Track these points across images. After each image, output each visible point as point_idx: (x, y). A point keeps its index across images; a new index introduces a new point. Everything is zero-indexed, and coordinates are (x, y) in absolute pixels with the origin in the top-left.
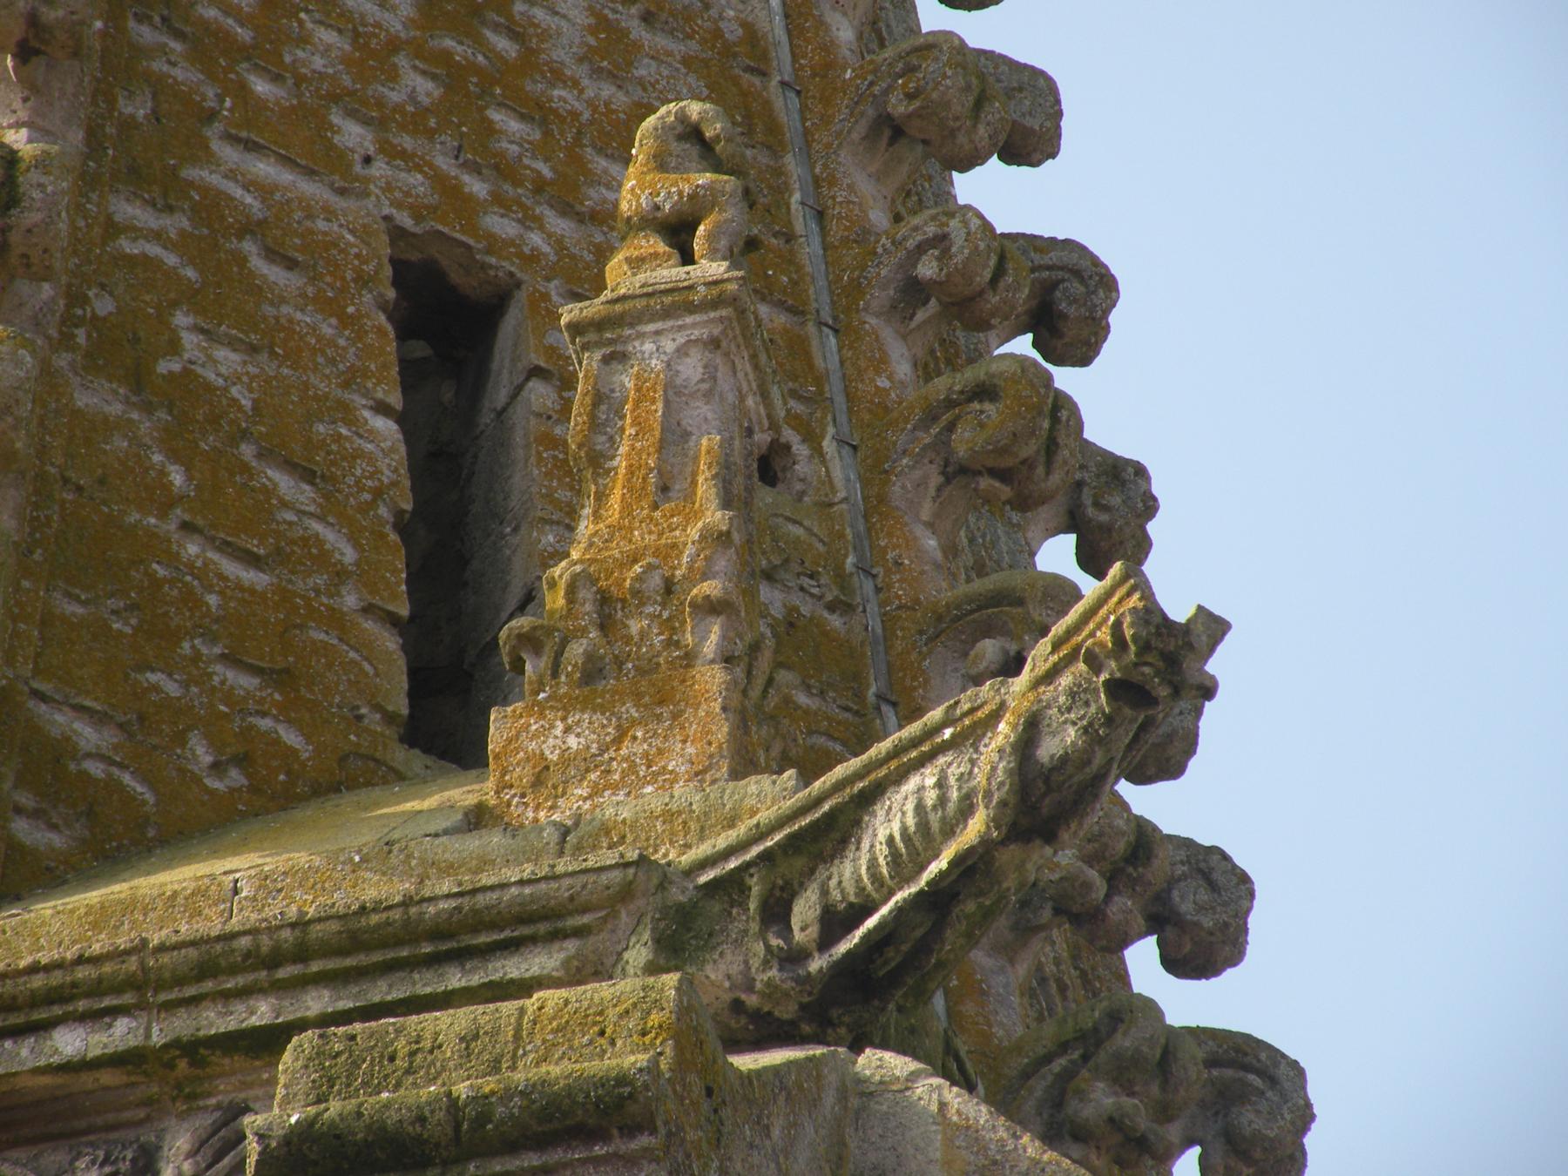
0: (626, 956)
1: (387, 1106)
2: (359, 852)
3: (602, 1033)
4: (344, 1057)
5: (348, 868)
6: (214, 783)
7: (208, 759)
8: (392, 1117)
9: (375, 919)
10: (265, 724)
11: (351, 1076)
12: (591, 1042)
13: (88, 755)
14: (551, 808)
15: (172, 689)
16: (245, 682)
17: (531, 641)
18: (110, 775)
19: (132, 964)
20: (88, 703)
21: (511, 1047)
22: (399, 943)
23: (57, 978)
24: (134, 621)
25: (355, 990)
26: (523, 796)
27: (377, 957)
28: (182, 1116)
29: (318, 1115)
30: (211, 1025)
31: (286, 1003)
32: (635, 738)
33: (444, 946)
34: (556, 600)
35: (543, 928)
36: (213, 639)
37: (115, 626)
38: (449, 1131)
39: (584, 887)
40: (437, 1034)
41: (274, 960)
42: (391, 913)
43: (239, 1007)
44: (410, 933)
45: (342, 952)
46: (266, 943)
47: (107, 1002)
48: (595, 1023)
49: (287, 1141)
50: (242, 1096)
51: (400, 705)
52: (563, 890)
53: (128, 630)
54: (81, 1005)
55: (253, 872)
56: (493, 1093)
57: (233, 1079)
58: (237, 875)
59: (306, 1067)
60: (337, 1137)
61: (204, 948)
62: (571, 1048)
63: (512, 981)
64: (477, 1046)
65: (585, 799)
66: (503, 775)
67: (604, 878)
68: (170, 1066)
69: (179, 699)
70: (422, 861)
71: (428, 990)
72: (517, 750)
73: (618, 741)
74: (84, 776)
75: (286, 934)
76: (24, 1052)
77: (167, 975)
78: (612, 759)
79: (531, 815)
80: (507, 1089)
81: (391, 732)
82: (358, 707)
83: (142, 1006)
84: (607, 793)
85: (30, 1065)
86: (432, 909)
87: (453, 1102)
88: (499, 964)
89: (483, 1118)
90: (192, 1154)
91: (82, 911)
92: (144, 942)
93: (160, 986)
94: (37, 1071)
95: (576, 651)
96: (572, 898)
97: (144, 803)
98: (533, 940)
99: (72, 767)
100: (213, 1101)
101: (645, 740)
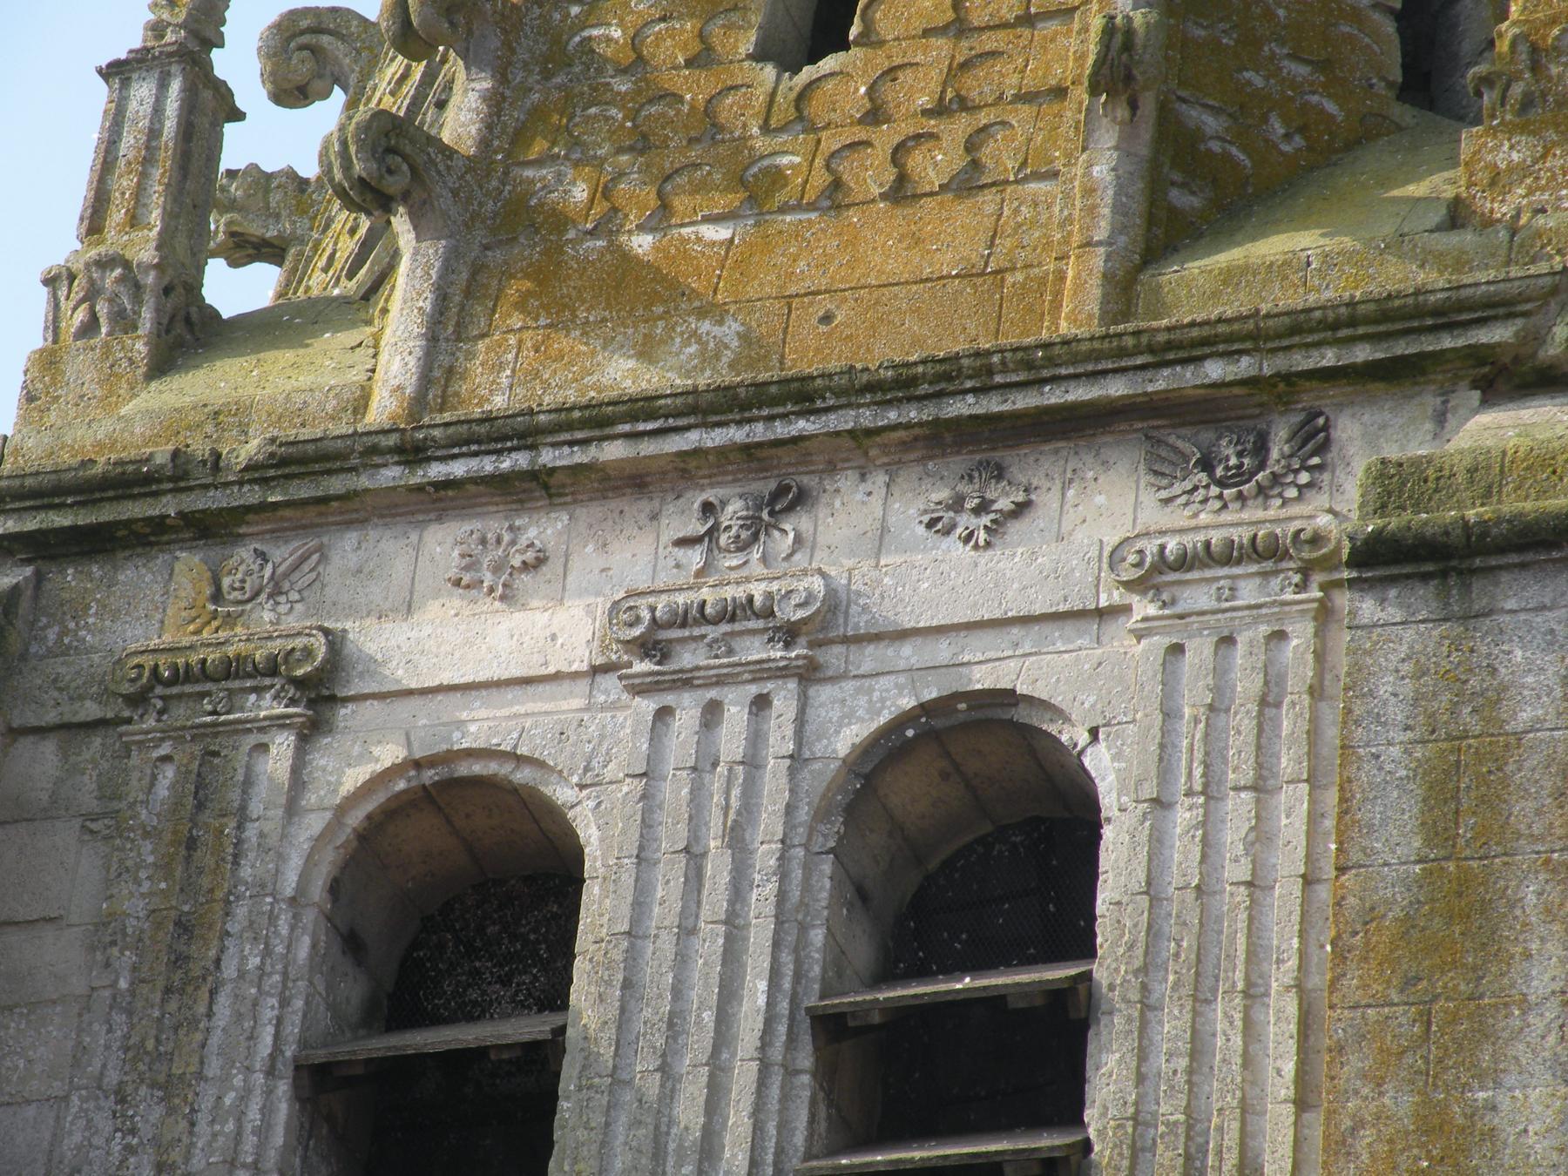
0: (1555, 329)
1: (1426, 523)
2: (1383, 241)
3: (1554, 472)
4: (1396, 478)
5: (1377, 252)
6: (1286, 148)
7: (1282, 131)
8: (1429, 531)
9: (1397, 303)
10: (1315, 99)
11: (1401, 492)
12: (1548, 478)
13: (1212, 138)
14: (1502, 201)
15: (1258, 81)
16: (1302, 70)
17: (1487, 81)
18: (1224, 149)
19: (1251, 325)
20: (1211, 102)
21: (1498, 478)
22: (1411, 317)
23: (1206, 331)
24: (1235, 36)
25: (1386, 345)
26: (1484, 192)
27: (1399, 326)
28: (1282, 414)
29: (1385, 526)
30: (1299, 364)
31: (1344, 352)
32: (1555, 155)
33: (1440, 321)
34: (1503, 46)
35: (1501, 311)
36: (1283, 45)
37: (1224, 41)
38: (1464, 540)
39: (1528, 287)
40: (1453, 466)
41: (1335, 326)
42: (1407, 299)
43: (1315, 353)
44: (1419, 312)
45: (1376, 322)
46: (1331, 315)
47: (1236, 347)
48: (1550, 465)
49: (1366, 542)
50: (1317, 403)
51: (1397, 75)
52: (1514, 288)
53: (1232, 43)
54: (1221, 347)
55: (1319, 251)
56: (1490, 520)
57: (1312, 394)
58: (1309, 252)
59: (1373, 483)
60: (1397, 541)
61: (1294, 317)
62: (1535, 481)
63: (1482, 344)
64: (1477, 476)
65: (1524, 197)
66: (1471, 177)
67: (1541, 282)
68: (1275, 386)
69: (1263, 89)
70: (1423, 249)
71: (1431, 348)
72: (1479, 160)
73: (1544, 157)
74: (1209, 150)
75: (1343, 310)
76: (1188, 375)
77: (1271, 333)
78: (1540, 169)
79: (1489, 205)
80: (1499, 518)
81: (1391, 94)
82: (1370, 79)
83: (1257, 349)
84: (1538, 193)
85: (1191, 383)
86: (1432, 298)
87: (1466, 523)
88: (1474, 333)
89: (1484, 534)
90: (1287, 442)
91: (1217, 272)
92: (1258, 311)
93: (1268, 338)
94: (1196, 387)
95: (1517, 90)
96: (1520, 294)
97: (1245, 167)
98: (1495, 318)
99: (1202, 147)
100: (1300, 406)
101: (1561, 157)
